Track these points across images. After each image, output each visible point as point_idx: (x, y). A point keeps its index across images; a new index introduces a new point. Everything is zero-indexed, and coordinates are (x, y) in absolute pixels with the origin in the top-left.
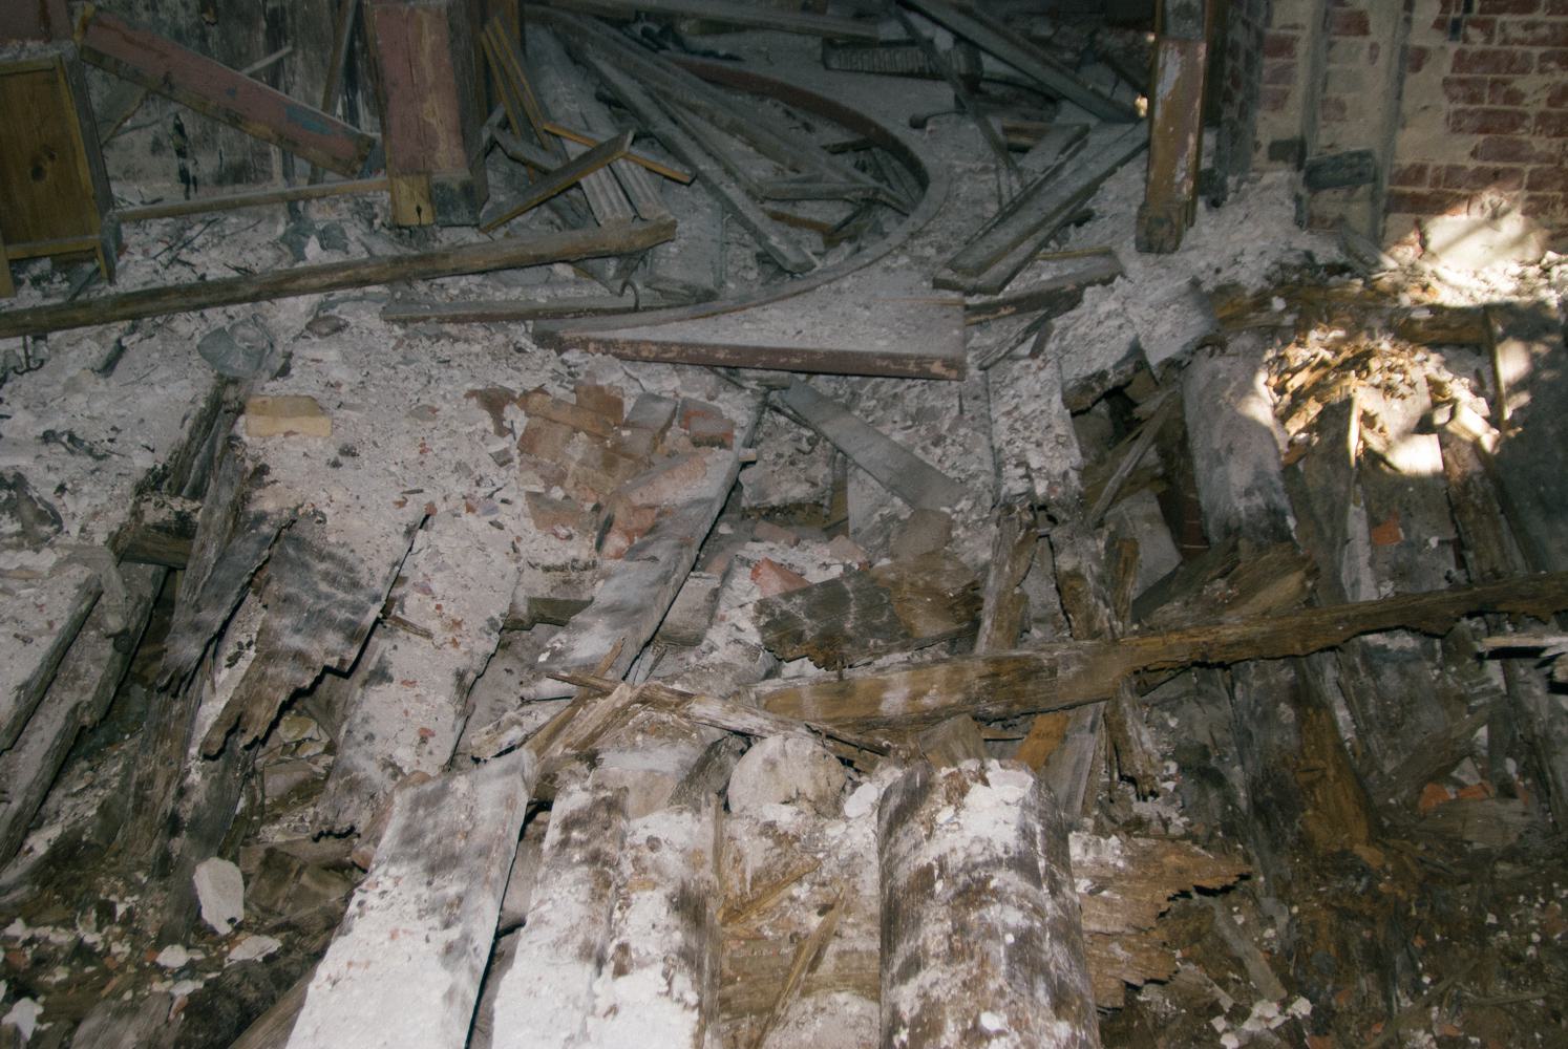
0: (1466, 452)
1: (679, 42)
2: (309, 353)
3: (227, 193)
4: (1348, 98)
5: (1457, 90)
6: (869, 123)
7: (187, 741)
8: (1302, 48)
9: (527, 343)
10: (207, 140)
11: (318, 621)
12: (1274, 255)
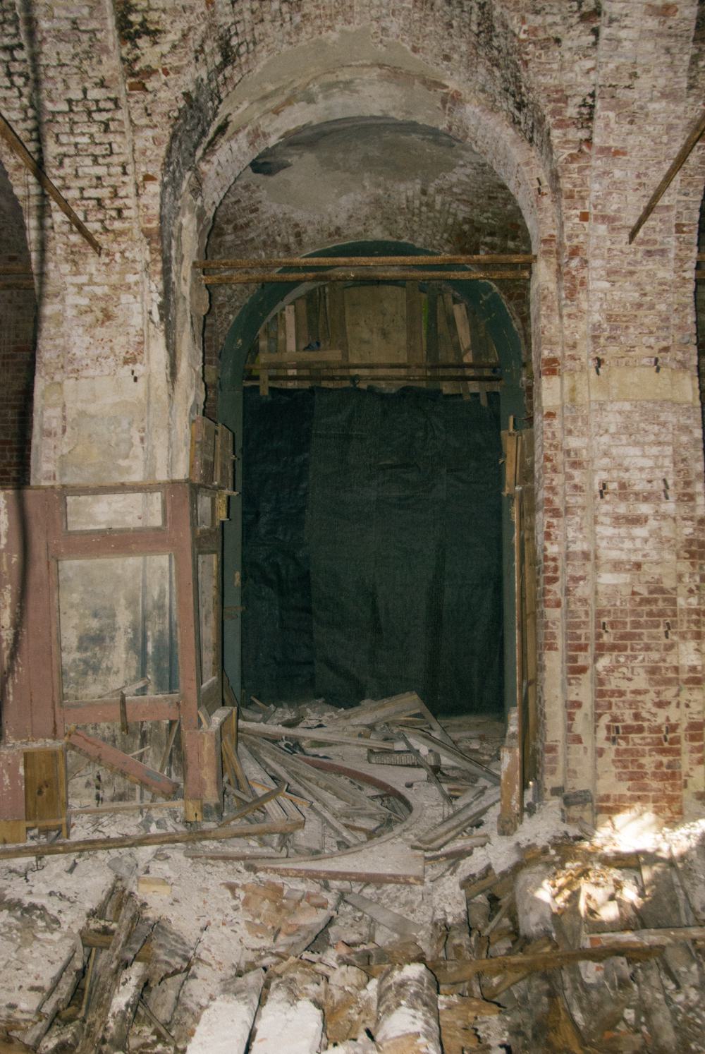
0: (629, 908)
1: (302, 750)
2: (157, 866)
3: (115, 805)
4: (578, 769)
5: (619, 764)
6: (388, 786)
7: (108, 1010)
8: (560, 750)
9: (241, 868)
10: (110, 782)
11: (173, 953)
12: (552, 833)
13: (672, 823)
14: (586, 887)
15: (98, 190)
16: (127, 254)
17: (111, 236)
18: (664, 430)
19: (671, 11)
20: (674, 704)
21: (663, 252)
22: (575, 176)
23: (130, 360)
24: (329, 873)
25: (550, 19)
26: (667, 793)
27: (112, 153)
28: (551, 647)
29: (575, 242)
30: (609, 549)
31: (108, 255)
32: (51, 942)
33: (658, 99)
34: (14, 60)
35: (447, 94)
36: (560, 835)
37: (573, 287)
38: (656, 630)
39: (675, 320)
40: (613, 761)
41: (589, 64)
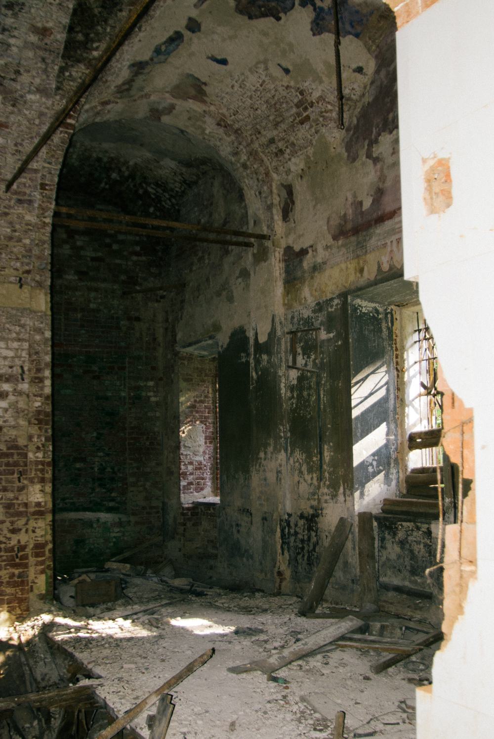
13: (21, 619)
18: (23, 330)
19: (48, 33)
20: (24, 530)
21: (30, 202)
26: (18, 596)
33: (34, 93)
38: (11, 477)
39: (36, 251)
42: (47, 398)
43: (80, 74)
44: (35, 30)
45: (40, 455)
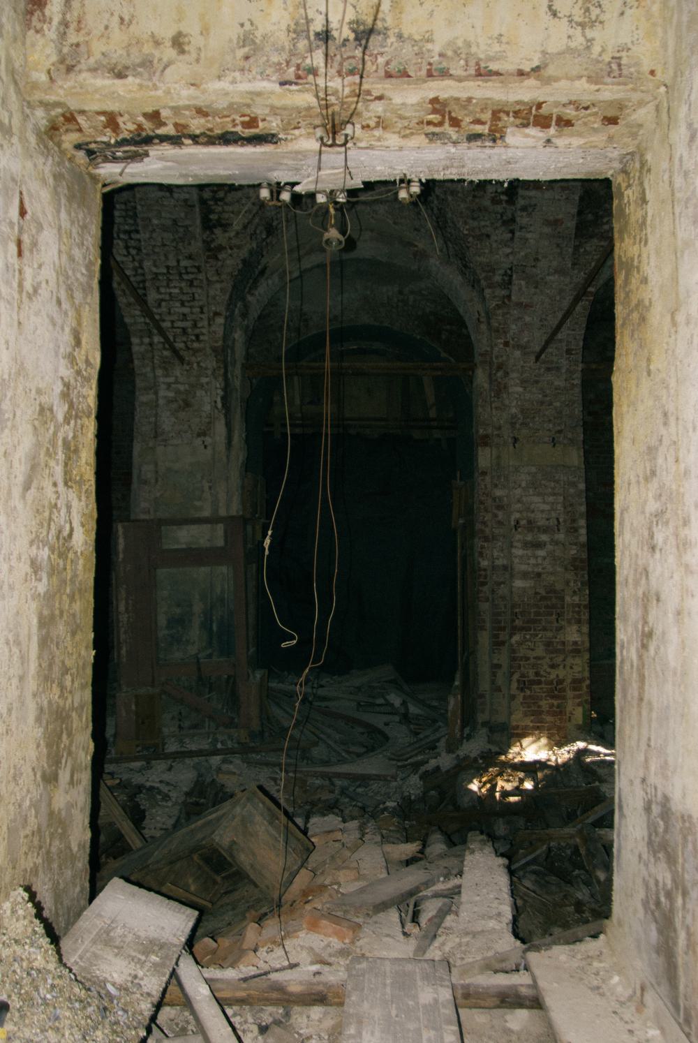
13: (560, 745)
14: (501, 783)
15: (184, 323)
16: (202, 364)
17: (191, 352)
20: (561, 667)
21: (558, 369)
22: (500, 318)
23: (202, 434)
24: (334, 773)
25: (483, 223)
27: (194, 299)
28: (483, 628)
29: (500, 360)
30: (521, 564)
31: (188, 364)
32: (167, 807)
34: (131, 239)
35: (417, 251)
36: (485, 751)
37: (499, 390)
40: (522, 703)
41: (508, 250)
42: (582, 546)
43: (594, 247)
44: (548, 223)
45: (576, 599)
